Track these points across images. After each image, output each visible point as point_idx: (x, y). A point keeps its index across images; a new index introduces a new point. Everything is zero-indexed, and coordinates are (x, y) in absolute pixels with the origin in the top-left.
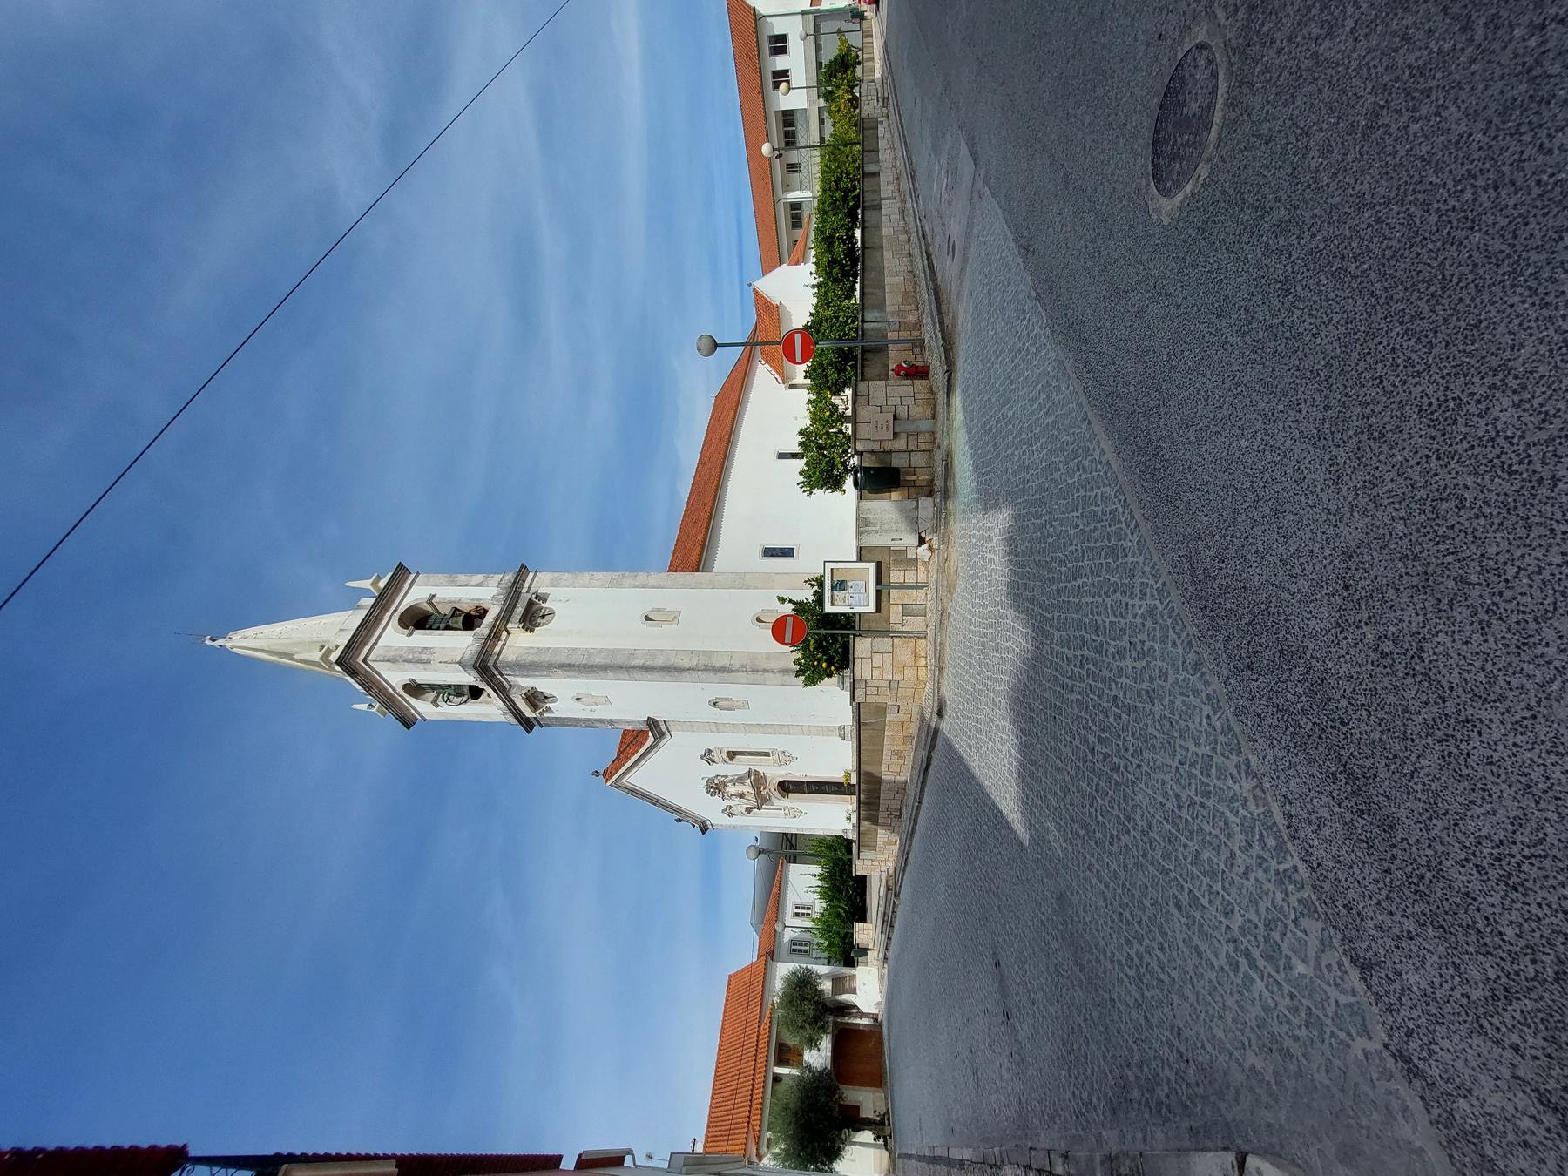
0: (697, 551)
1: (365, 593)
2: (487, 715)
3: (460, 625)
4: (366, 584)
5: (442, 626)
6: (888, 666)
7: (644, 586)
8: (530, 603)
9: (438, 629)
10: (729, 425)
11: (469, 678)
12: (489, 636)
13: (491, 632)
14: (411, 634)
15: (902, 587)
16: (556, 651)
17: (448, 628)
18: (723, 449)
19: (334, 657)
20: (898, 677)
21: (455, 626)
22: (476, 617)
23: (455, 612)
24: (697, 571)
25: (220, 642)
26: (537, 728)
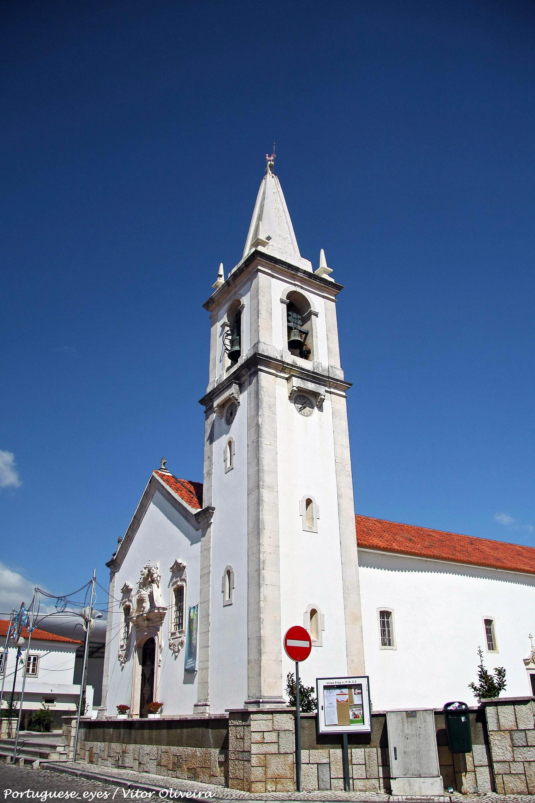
0: (525, 568)
1: (316, 265)
2: (328, 331)
3: (293, 338)
4: (323, 262)
5: (291, 324)
6: (266, 748)
7: (339, 496)
8: (316, 395)
9: (288, 321)
10: (514, 565)
11: (245, 354)
12: (283, 362)
13: (288, 364)
14: (282, 302)
15: (346, 762)
16: (274, 421)
17: (290, 329)
18: (488, 562)
19: (260, 249)
20: (254, 760)
21: (292, 334)
22: (301, 349)
23: (304, 333)
24: (359, 545)
25: (269, 171)
26: (204, 408)
